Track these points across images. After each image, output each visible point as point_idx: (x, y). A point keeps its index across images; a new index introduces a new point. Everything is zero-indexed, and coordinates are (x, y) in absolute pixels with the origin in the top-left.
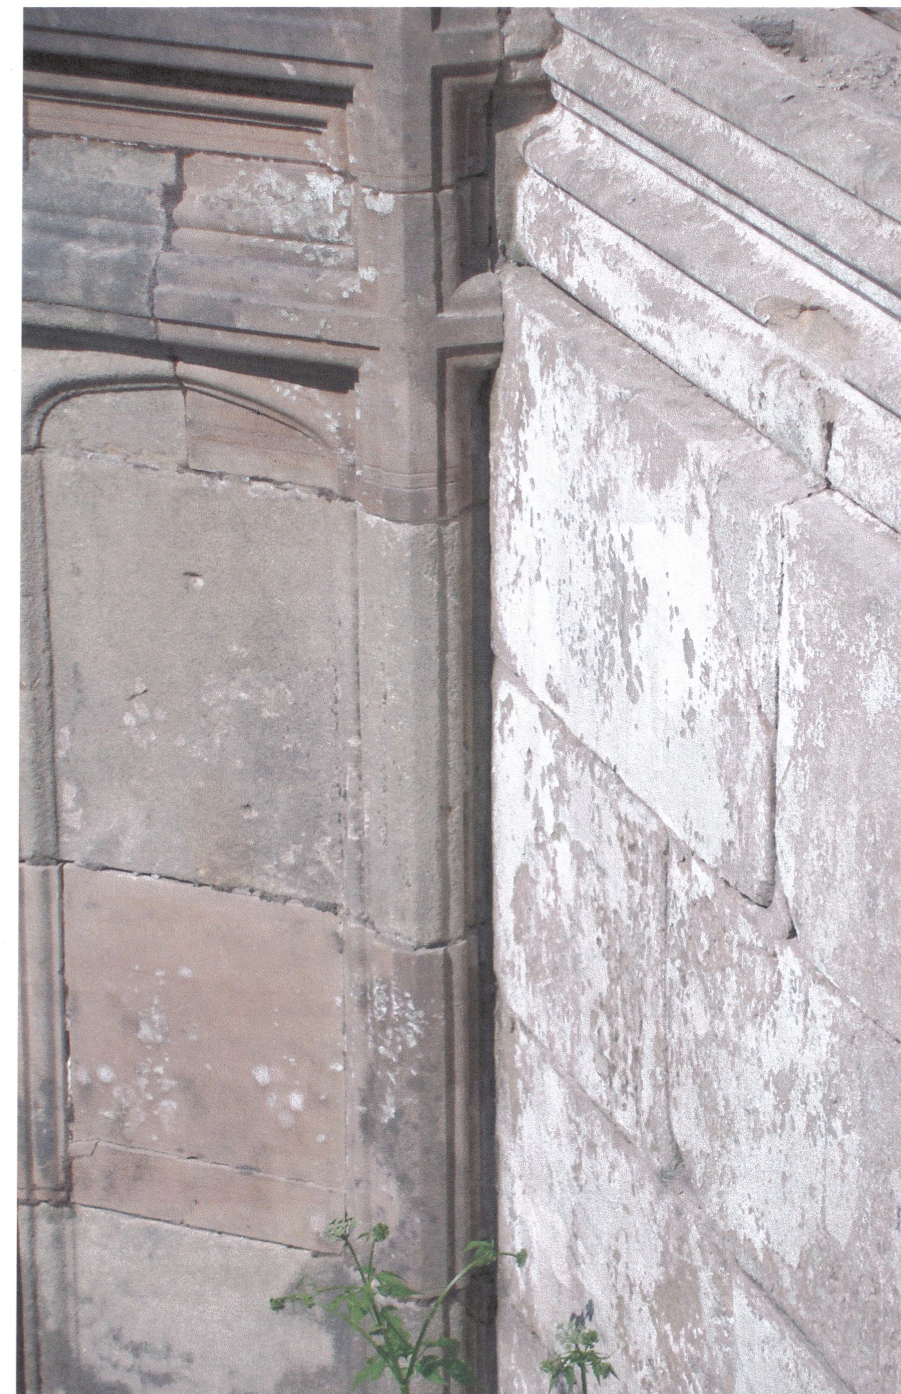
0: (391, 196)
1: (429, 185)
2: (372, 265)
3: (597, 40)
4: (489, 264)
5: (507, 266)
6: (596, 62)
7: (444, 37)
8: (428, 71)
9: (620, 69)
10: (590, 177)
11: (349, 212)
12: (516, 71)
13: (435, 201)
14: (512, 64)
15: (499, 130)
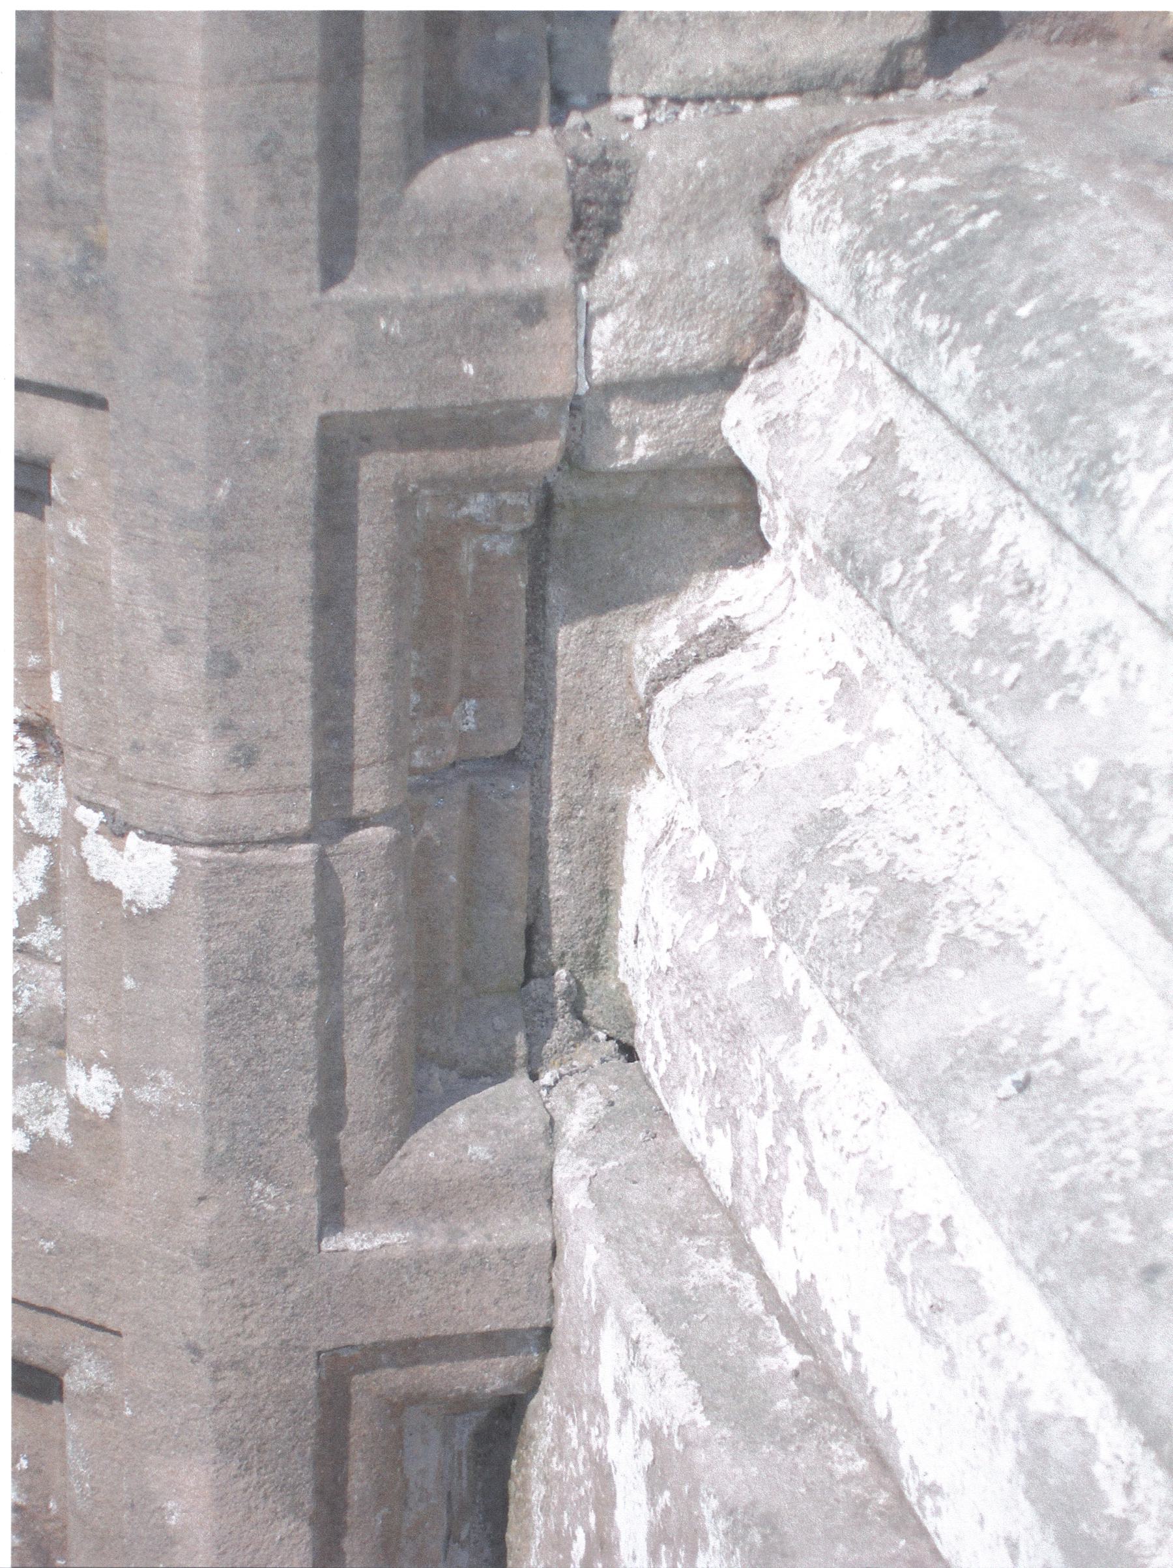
0: (166, 849)
1: (300, 821)
2: (103, 1065)
3: (919, 379)
4: (521, 1051)
5: (584, 1056)
6: (908, 456)
7: (363, 313)
8: (307, 430)
9: (999, 511)
10: (859, 900)
11: (54, 855)
12: (632, 434)
13: (325, 871)
14: (617, 408)
15: (572, 617)
